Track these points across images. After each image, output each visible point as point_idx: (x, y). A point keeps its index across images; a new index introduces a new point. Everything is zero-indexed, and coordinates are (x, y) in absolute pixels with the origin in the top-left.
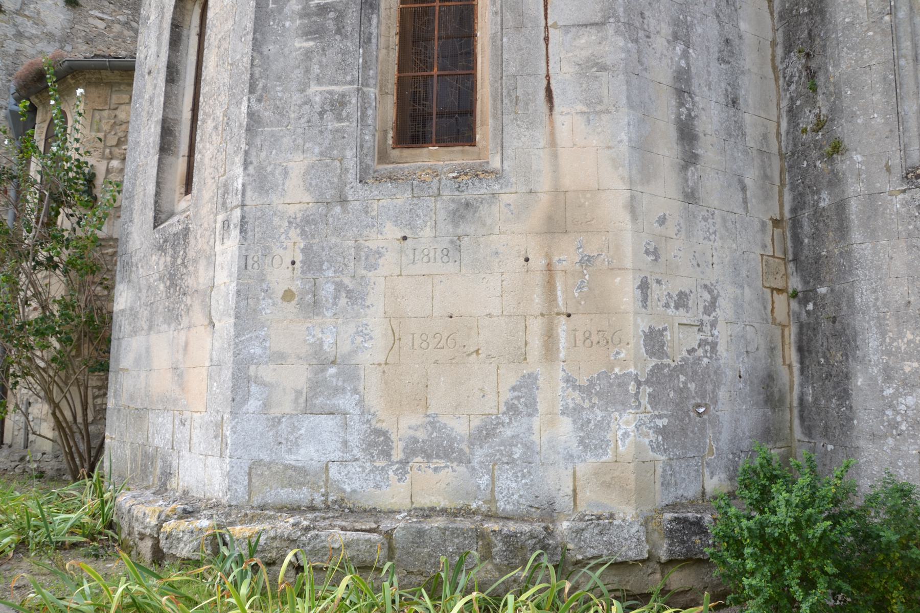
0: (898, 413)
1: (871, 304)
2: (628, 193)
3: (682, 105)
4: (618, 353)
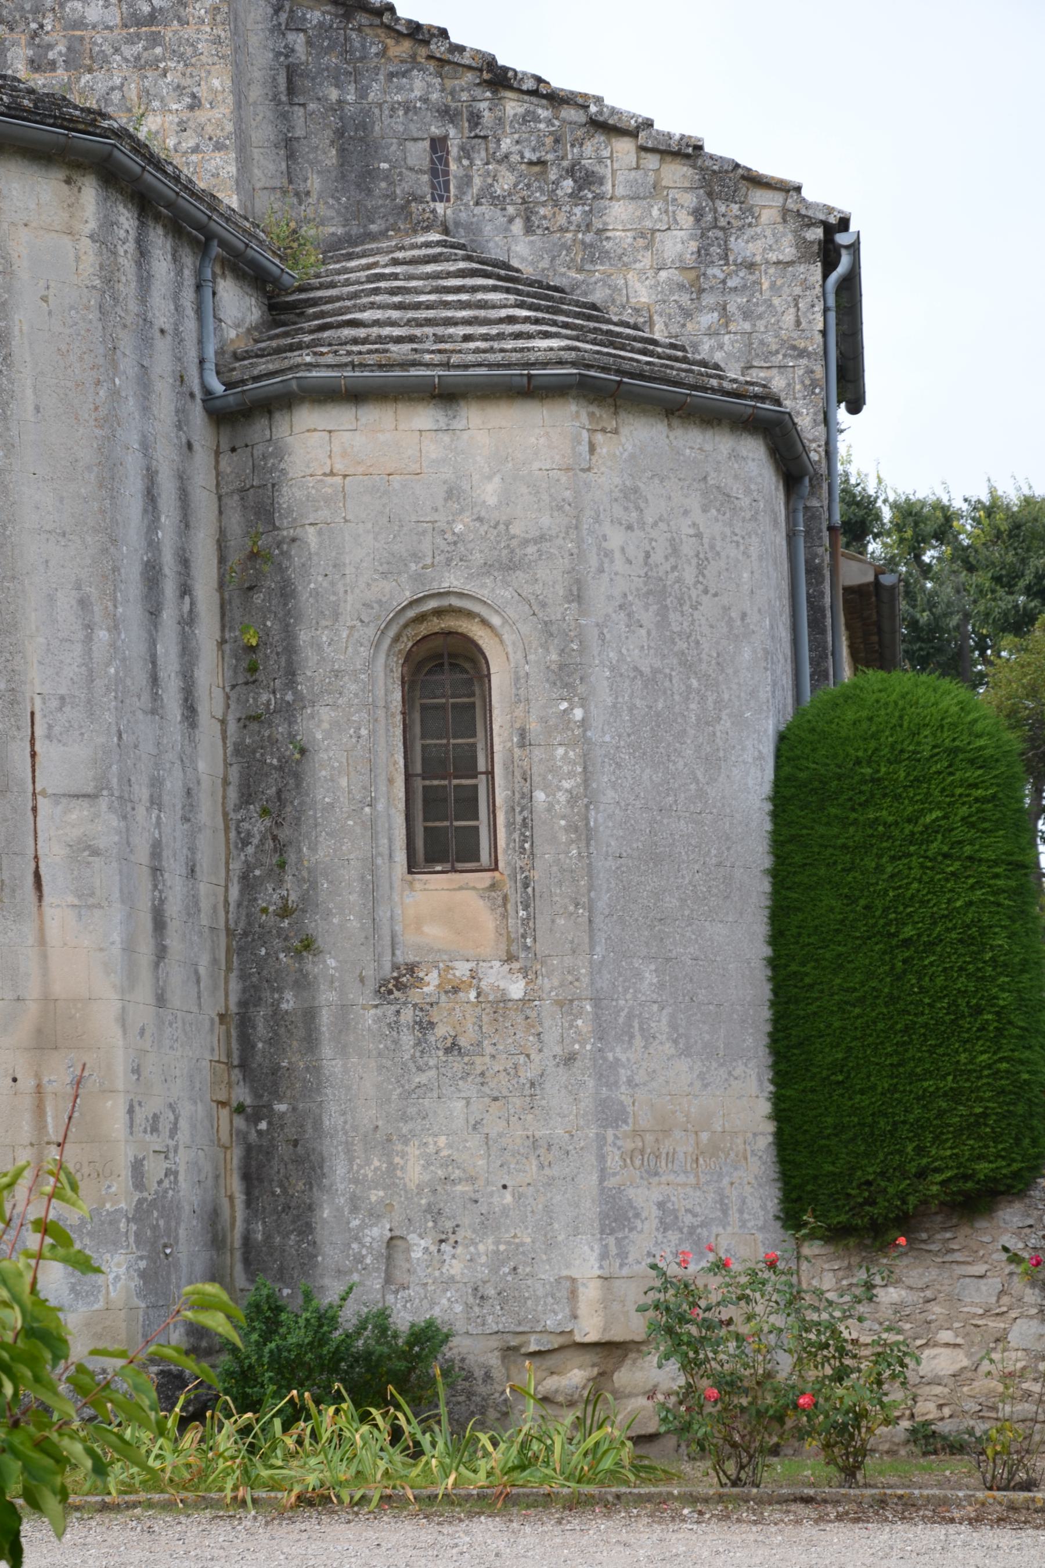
0: (364, 1246)
1: (339, 1128)
2: (119, 1004)
3: (155, 886)
4: (109, 1187)
